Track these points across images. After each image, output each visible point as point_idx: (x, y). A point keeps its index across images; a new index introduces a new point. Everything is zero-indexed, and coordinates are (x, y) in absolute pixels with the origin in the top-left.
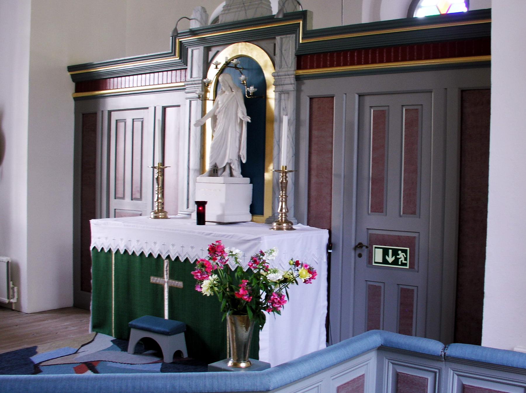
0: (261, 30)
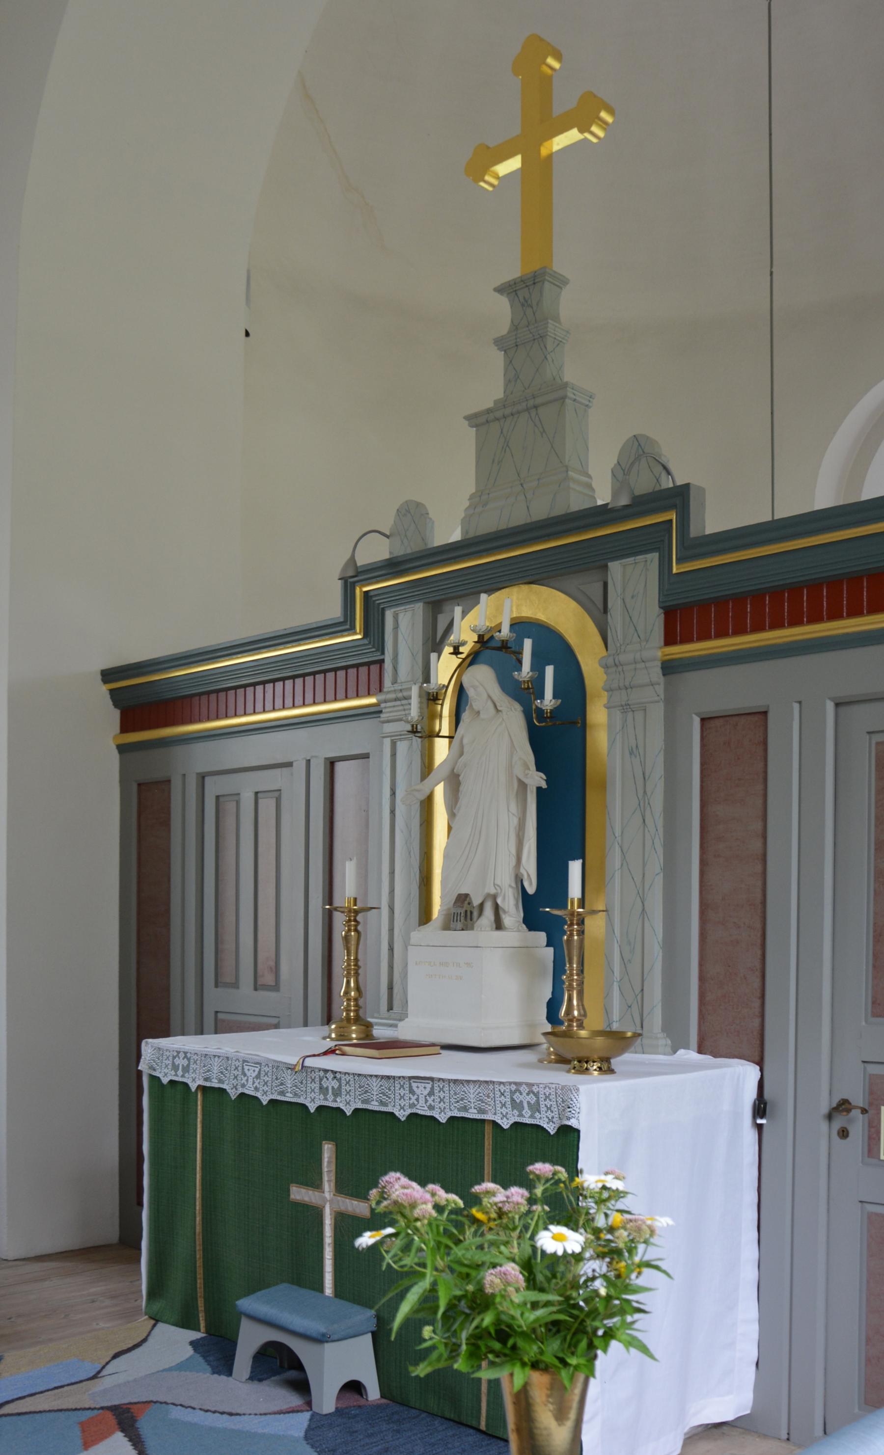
0: (567, 547)
